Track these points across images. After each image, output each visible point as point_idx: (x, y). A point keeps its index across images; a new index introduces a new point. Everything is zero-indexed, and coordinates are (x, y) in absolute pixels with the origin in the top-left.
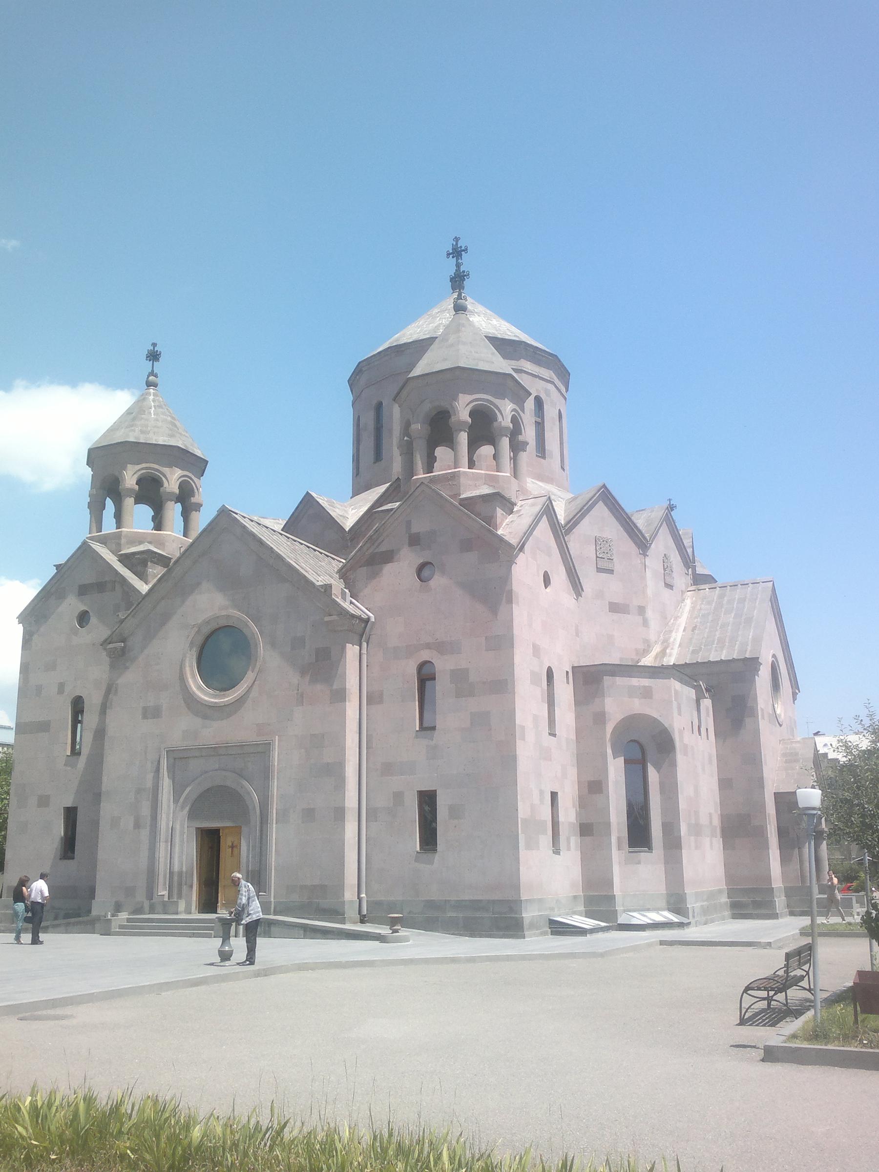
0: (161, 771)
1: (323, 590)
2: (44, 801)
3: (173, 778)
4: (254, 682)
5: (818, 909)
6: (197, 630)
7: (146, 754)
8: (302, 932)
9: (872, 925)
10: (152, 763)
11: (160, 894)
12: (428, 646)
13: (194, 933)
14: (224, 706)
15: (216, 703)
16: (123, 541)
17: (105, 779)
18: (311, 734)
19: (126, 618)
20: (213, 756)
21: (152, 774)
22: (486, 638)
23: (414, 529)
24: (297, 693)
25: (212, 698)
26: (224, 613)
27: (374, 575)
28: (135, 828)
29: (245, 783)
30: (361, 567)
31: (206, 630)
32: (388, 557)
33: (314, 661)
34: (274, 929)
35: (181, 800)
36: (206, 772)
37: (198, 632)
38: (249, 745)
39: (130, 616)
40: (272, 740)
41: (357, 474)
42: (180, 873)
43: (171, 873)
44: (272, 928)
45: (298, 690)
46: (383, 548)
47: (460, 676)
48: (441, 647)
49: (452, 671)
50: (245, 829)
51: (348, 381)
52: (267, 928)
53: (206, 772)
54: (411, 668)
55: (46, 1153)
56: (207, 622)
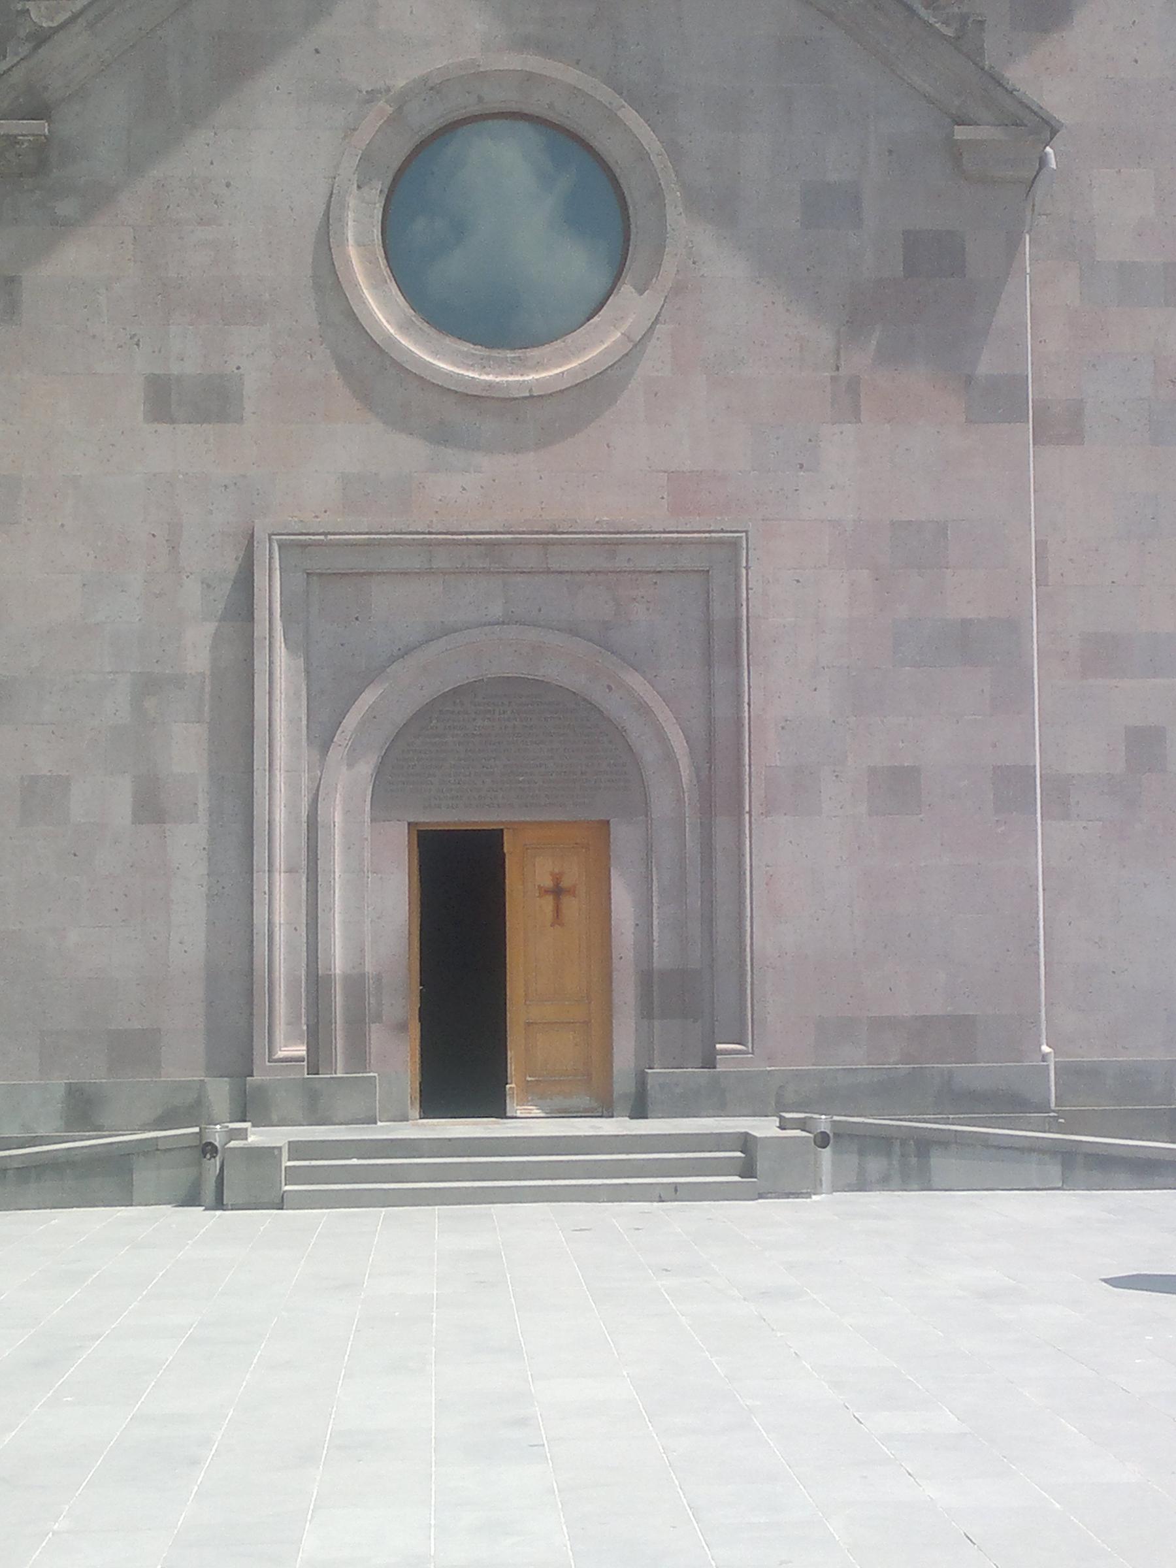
0: (261, 614)
1: (949, 32)
3: (301, 645)
4: (651, 329)
6: (390, 110)
7: (174, 548)
8: (1055, 1170)
9: (1061, 1123)
11: (281, 1054)
13: (676, 1187)
14: (525, 398)
15: (490, 385)
18: (893, 524)
19: (62, 26)
20: (487, 572)
21: (210, 627)
24: (832, 378)
25: (470, 367)
26: (513, 61)
28: (137, 819)
29: (635, 680)
31: (425, 118)
34: (937, 1161)
35: (351, 721)
36: (448, 631)
37: (397, 119)
38: (646, 542)
39: (81, 21)
40: (746, 532)
42: (356, 984)
44: (934, 1161)
45: (838, 369)
50: (624, 836)
52: (914, 1160)
53: (448, 631)
56: (432, 88)
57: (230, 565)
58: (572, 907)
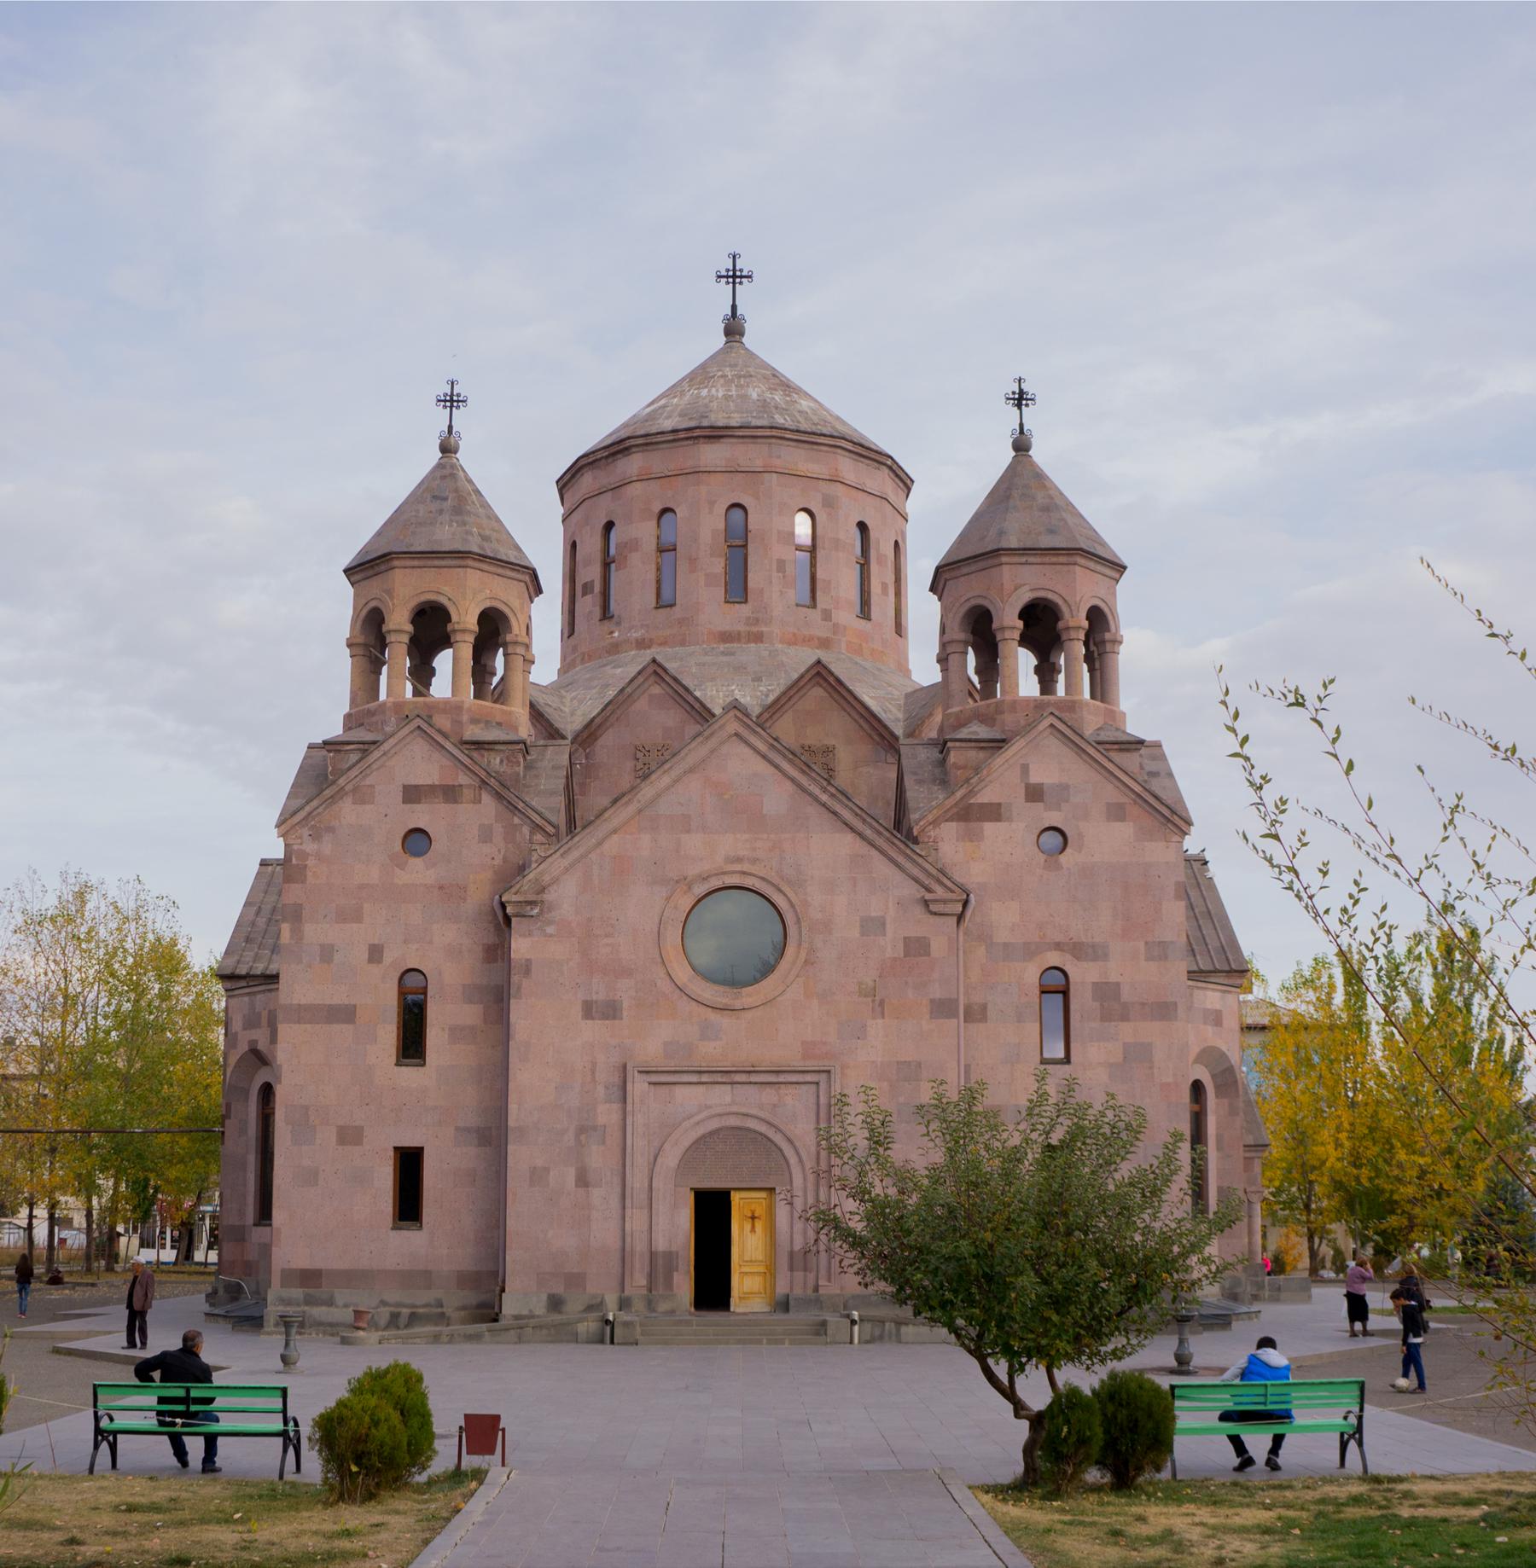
2: (350, 1136)
5: (358, 1500)
10: (607, 1088)
12: (1058, 946)
16: (465, 718)
17: (513, 1108)
18: (898, 1062)
22: (1146, 943)
23: (1034, 778)
27: (973, 837)
28: (577, 1186)
30: (946, 821)
32: (994, 812)
33: (902, 955)
41: (571, 632)
43: (653, 1255)
46: (985, 797)
47: (1106, 992)
48: (1078, 950)
49: (1095, 984)
51: (557, 482)
54: (1031, 974)
55: (1485, 1504)
57: (616, 1079)
58: (759, 1225)
